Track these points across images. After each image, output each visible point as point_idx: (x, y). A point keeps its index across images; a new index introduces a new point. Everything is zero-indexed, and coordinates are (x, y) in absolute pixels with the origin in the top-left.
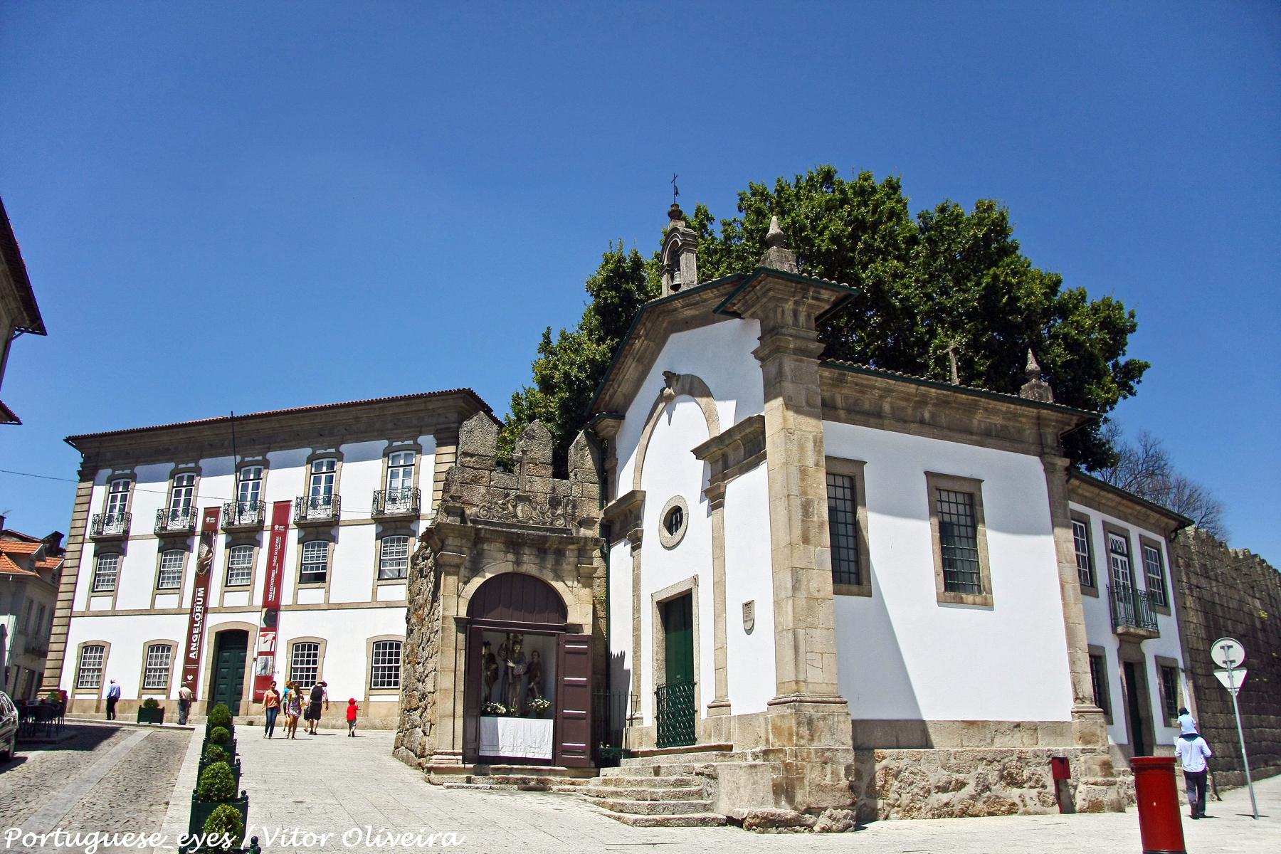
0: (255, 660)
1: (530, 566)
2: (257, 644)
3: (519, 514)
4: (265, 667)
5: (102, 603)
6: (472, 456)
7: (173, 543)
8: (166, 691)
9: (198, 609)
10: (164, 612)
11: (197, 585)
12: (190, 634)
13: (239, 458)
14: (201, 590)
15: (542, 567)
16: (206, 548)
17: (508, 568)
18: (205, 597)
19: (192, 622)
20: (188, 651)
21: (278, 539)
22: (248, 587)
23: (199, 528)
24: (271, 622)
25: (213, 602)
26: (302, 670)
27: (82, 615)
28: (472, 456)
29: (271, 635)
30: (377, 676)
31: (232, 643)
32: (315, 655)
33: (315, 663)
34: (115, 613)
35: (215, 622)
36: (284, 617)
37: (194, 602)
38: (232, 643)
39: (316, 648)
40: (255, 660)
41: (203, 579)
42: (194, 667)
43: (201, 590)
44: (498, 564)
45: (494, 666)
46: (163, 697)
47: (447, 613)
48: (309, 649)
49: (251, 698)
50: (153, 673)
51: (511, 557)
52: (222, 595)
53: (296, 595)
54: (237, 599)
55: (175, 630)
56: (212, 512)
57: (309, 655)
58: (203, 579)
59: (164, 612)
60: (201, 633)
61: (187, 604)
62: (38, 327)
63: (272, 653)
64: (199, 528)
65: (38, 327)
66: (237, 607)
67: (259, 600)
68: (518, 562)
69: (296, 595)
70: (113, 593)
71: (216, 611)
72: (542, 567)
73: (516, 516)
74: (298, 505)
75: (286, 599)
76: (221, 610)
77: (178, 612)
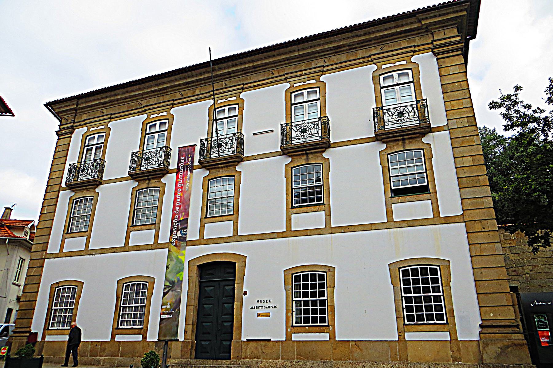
5: (76, 243)
8: (143, 332)
27: (56, 256)
33: (322, 294)
34: (87, 252)
39: (321, 277)
52: (202, 226)
66: (210, 241)
70: (87, 233)
74: (202, 147)
77: (438, 219)
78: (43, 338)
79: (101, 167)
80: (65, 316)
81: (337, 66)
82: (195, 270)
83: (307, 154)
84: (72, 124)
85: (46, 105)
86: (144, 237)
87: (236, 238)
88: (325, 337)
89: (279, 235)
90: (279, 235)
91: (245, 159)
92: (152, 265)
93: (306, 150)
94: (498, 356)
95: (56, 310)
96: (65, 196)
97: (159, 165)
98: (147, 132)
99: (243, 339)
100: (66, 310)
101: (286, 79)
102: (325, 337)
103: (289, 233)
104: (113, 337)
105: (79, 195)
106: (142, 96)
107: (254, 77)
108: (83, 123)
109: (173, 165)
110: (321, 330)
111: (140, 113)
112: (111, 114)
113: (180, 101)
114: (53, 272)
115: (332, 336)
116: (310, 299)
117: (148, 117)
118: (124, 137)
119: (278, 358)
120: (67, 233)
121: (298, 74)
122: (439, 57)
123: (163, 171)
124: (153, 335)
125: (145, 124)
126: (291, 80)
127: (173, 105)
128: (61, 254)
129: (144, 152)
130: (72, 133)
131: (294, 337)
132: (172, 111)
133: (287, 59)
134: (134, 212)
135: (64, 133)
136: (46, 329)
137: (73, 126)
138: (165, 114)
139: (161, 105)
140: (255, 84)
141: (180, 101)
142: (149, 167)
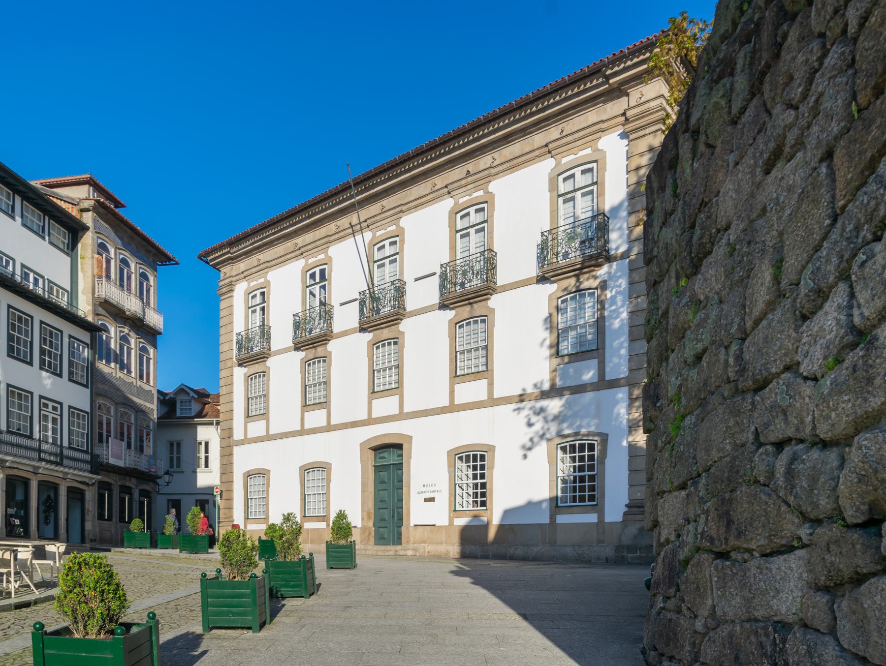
5: (257, 428)
8: (599, 509)
27: (241, 443)
32: (483, 467)
33: (483, 476)
39: (483, 458)
70: (264, 415)
78: (245, 527)
79: (490, 265)
81: (508, 165)
83: (470, 304)
87: (402, 416)
89: (442, 410)
90: (442, 410)
91: (498, 290)
94: (635, 537)
99: (412, 525)
103: (452, 408)
108: (242, 276)
113: (337, 236)
117: (558, 164)
119: (442, 543)
122: (632, 137)
125: (454, 213)
128: (246, 441)
130: (232, 291)
132: (493, 187)
136: (247, 518)
138: (481, 193)
139: (318, 243)
141: (337, 236)
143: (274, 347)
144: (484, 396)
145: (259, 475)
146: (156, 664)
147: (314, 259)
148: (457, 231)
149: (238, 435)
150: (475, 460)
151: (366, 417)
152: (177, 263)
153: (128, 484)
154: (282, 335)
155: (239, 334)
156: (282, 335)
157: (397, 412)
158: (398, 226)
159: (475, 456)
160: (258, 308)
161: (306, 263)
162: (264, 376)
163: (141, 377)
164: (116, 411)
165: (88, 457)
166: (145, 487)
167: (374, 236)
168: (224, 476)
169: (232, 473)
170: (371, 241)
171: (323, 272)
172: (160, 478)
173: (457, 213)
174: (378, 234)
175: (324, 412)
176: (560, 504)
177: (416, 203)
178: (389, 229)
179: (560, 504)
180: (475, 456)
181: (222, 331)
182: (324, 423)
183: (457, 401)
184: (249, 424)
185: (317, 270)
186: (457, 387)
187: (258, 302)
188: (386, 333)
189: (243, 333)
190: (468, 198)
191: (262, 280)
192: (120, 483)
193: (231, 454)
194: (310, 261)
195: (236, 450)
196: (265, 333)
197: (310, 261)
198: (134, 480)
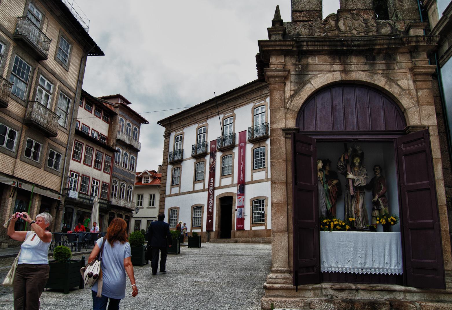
0: (236, 210)
1: (358, 72)
2: (236, 204)
3: (342, 27)
4: (241, 214)
5: (175, 190)
6: (301, 12)
7: (198, 157)
8: (201, 228)
9: (211, 188)
10: (198, 191)
11: (210, 177)
12: (209, 200)
13: (222, 116)
14: (212, 179)
15: (372, 72)
16: (212, 159)
17: (337, 77)
18: (214, 183)
19: (209, 194)
20: (208, 208)
21: (242, 150)
22: (231, 175)
23: (209, 151)
24: (242, 191)
25: (217, 185)
26: (258, 214)
27: (169, 196)
28: (301, 12)
29: (243, 197)
30: (255, 207)
31: (226, 202)
32: (263, 206)
33: (263, 209)
34: (180, 194)
35: (218, 193)
36: (247, 187)
37: (209, 185)
38: (226, 202)
39: (263, 202)
40: (236, 210)
41: (212, 175)
42: (209, 216)
43: (212, 179)
44: (323, 74)
45: (335, 182)
46: (199, 231)
47: (275, 126)
48: (260, 203)
49: (235, 230)
50: (196, 221)
51: (337, 67)
52: (220, 180)
53: (252, 176)
54: (227, 181)
55: (202, 199)
56: (213, 142)
57: (260, 206)
58: (212, 175)
59: (198, 191)
60: (213, 200)
61: (207, 187)
62: (98, 52)
63: (243, 206)
64: (209, 151)
65: (98, 52)
66: (227, 186)
67: (236, 181)
68: (345, 71)
69: (252, 176)
70: (179, 185)
71: (219, 188)
72: (372, 72)
73: (338, 28)
74: (249, 132)
75: (248, 179)
76: (220, 187)
77: (204, 190)
80: (199, 221)
82: (218, 199)
84: (169, 131)
85: (158, 123)
86: (199, 186)
88: (263, 228)
92: (202, 199)
93: (258, 140)
95: (171, 220)
96: (170, 167)
97: (263, 134)
98: (255, 114)
100: (175, 219)
101: (252, 102)
102: (199, 231)
104: (191, 231)
105: (175, 167)
106: (196, 114)
107: (240, 101)
109: (237, 142)
110: (261, 225)
111: (195, 123)
112: (184, 125)
114: (169, 203)
115: (266, 227)
116: (262, 211)
118: (190, 136)
119: (247, 237)
120: (254, 169)
121: (257, 98)
123: (233, 146)
124: (205, 229)
126: (254, 102)
127: (208, 118)
129: (255, 127)
131: (254, 228)
133: (252, 91)
134: (196, 175)
135: (167, 136)
137: (170, 132)
138: (232, 113)
139: (203, 119)
140: (240, 105)
142: (258, 135)
143: (184, 158)
144: (230, 183)
145: (174, 211)
146: (1, 268)
147: (178, 133)
148: (198, 135)
149: (168, 193)
150: (260, 203)
151: (192, 190)
152: (149, 123)
153: (121, 213)
154: (188, 153)
155: (171, 152)
156: (188, 153)
157: (231, 184)
158: (233, 113)
159: (260, 201)
160: (202, 135)
161: (199, 126)
162: (179, 169)
163: (130, 169)
164: (119, 183)
165: (106, 202)
166: (127, 214)
167: (224, 116)
168: (160, 210)
169: (164, 208)
170: (223, 118)
171: (181, 137)
172: (134, 210)
173: (254, 109)
174: (226, 115)
175: (203, 183)
176: (253, 223)
177: (240, 105)
178: (230, 114)
179: (253, 223)
180: (260, 201)
181: (2, 202)
182: (178, 192)
183: (254, 180)
184: (222, 180)
185: (179, 136)
186: (222, 180)
187: (202, 132)
188: (227, 153)
189: (172, 152)
190: (228, 115)
191: (181, 132)
192: (118, 213)
193: (164, 201)
194: (200, 125)
195: (167, 199)
196: (182, 152)
197: (200, 125)
198: (123, 212)
